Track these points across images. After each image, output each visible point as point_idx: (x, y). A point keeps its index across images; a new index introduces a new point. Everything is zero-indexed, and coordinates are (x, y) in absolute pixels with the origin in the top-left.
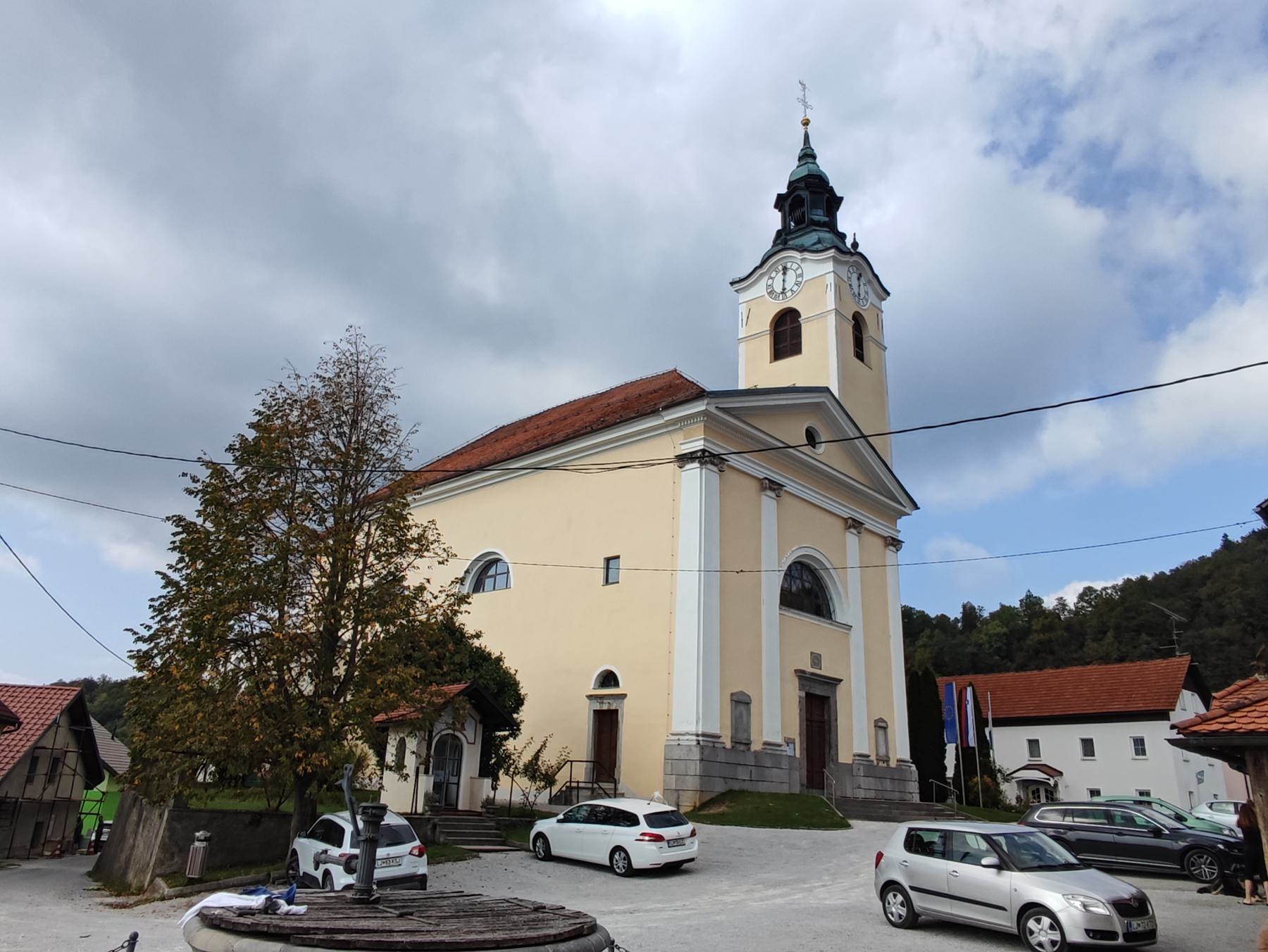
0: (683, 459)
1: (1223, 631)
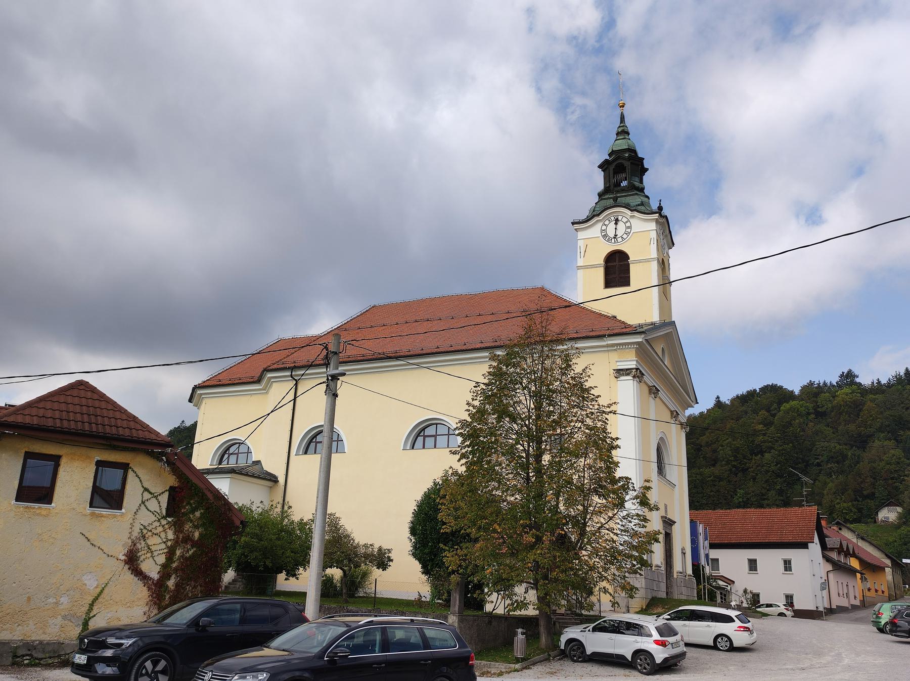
1: (716, 470)
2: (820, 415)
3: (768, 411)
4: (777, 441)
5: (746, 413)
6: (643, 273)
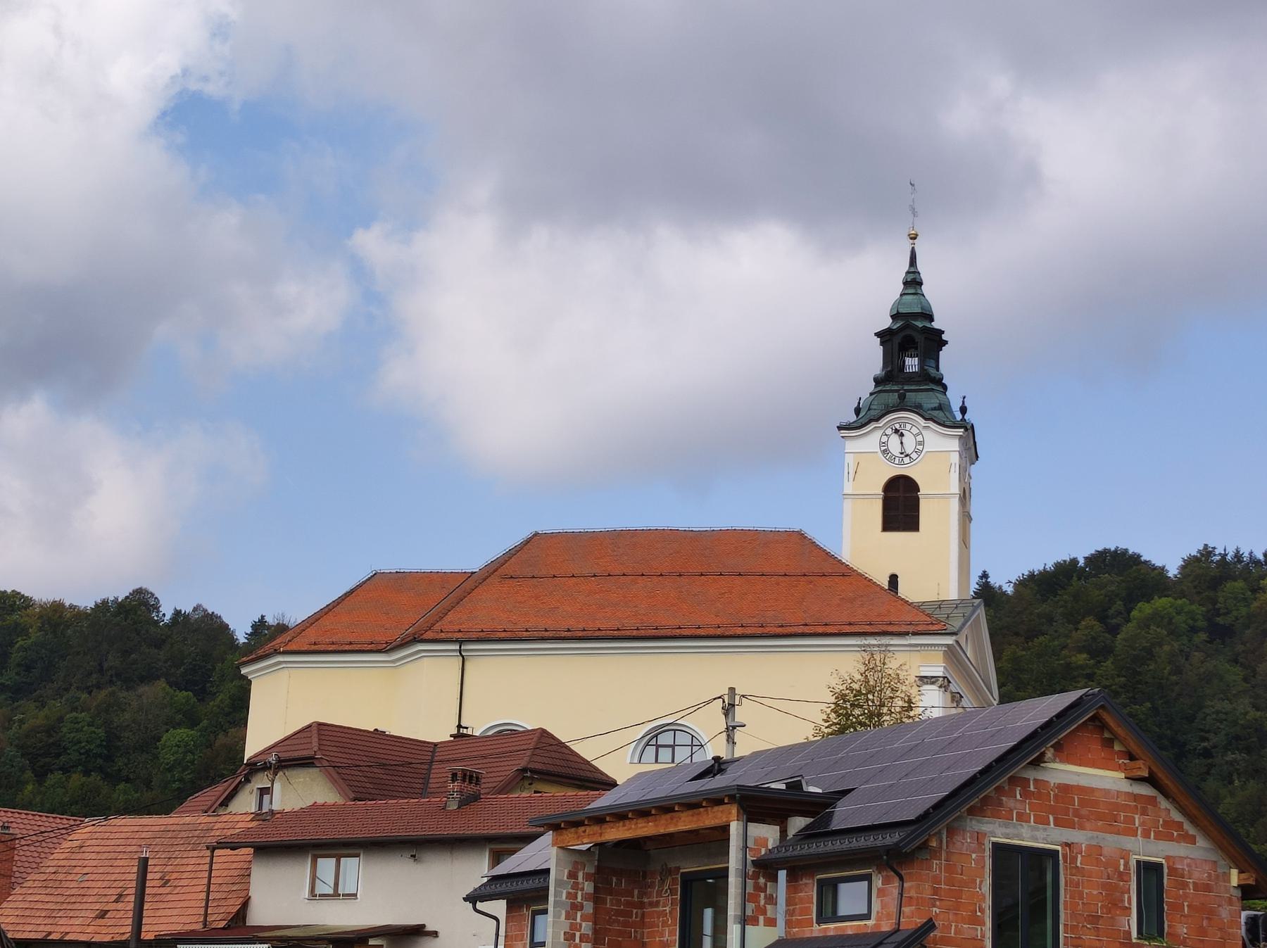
2: (1220, 633)
3: (1102, 618)
4: (1117, 694)
5: (1050, 620)
6: (938, 512)
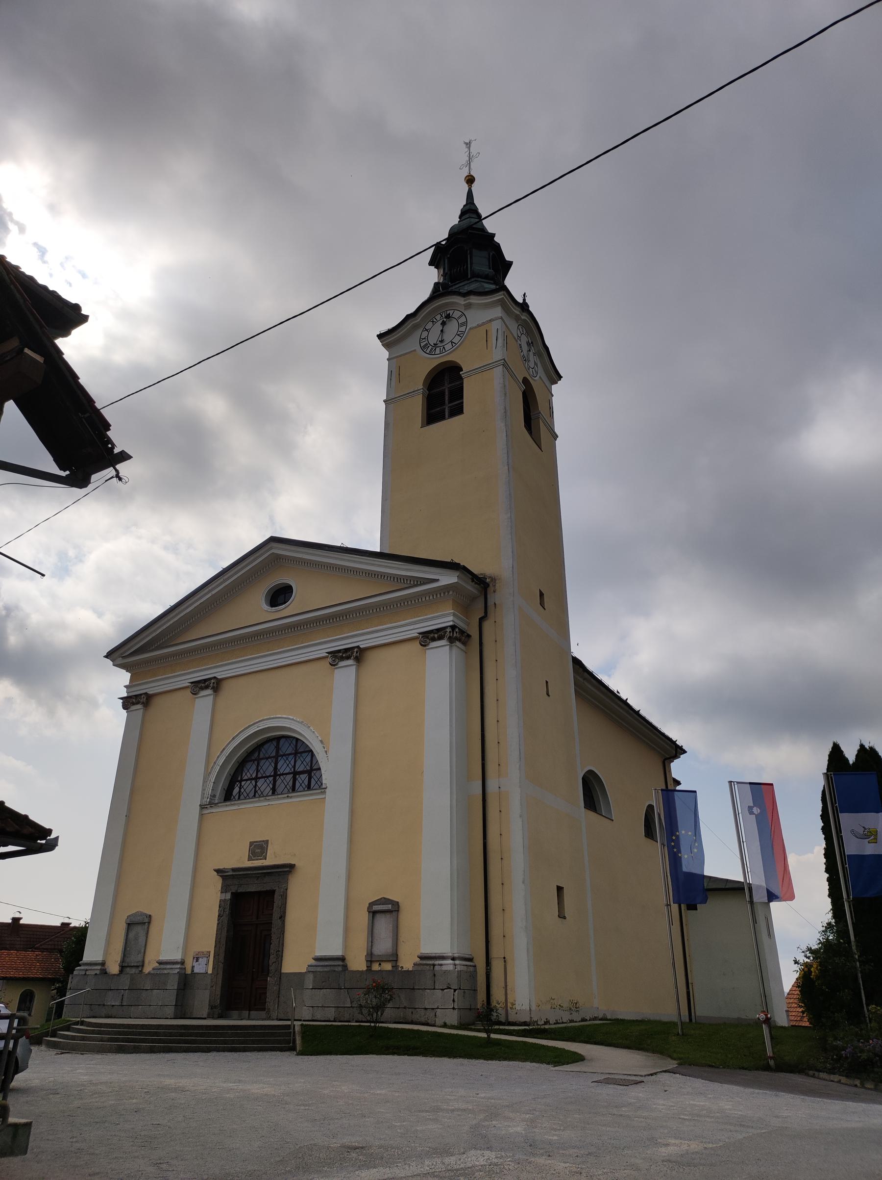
0: (428, 637)
